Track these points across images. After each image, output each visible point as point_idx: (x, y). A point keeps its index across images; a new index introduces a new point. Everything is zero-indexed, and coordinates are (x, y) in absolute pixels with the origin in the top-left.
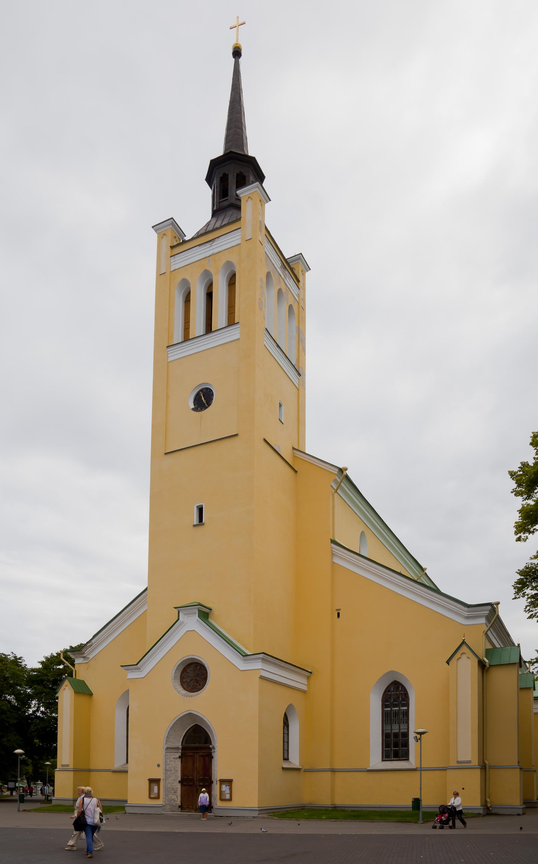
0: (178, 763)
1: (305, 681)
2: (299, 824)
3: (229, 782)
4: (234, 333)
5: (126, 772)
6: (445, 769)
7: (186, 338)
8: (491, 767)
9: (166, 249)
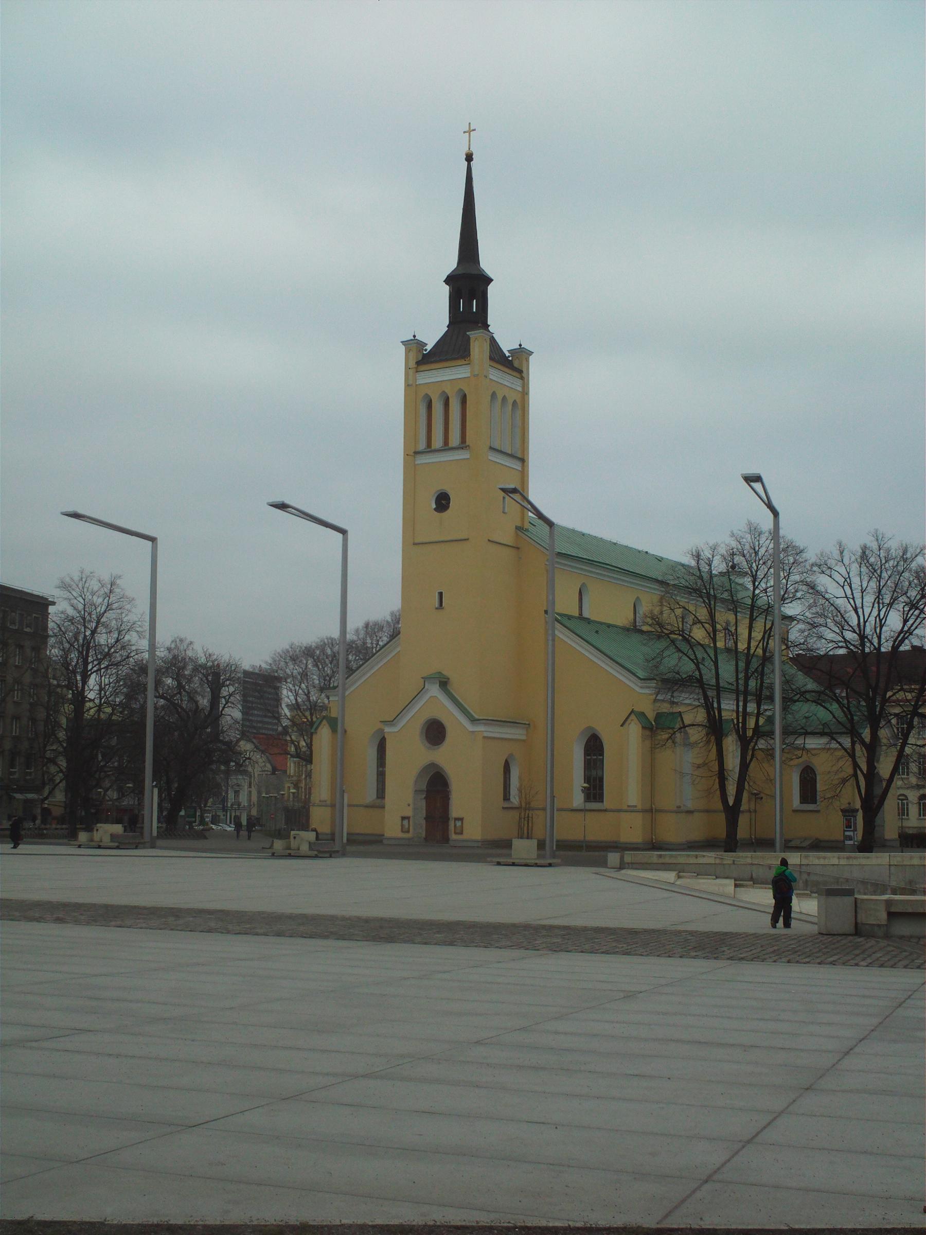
0: (424, 803)
3: (461, 819)
5: (383, 807)
6: (619, 811)
8: (656, 811)
9: (412, 364)
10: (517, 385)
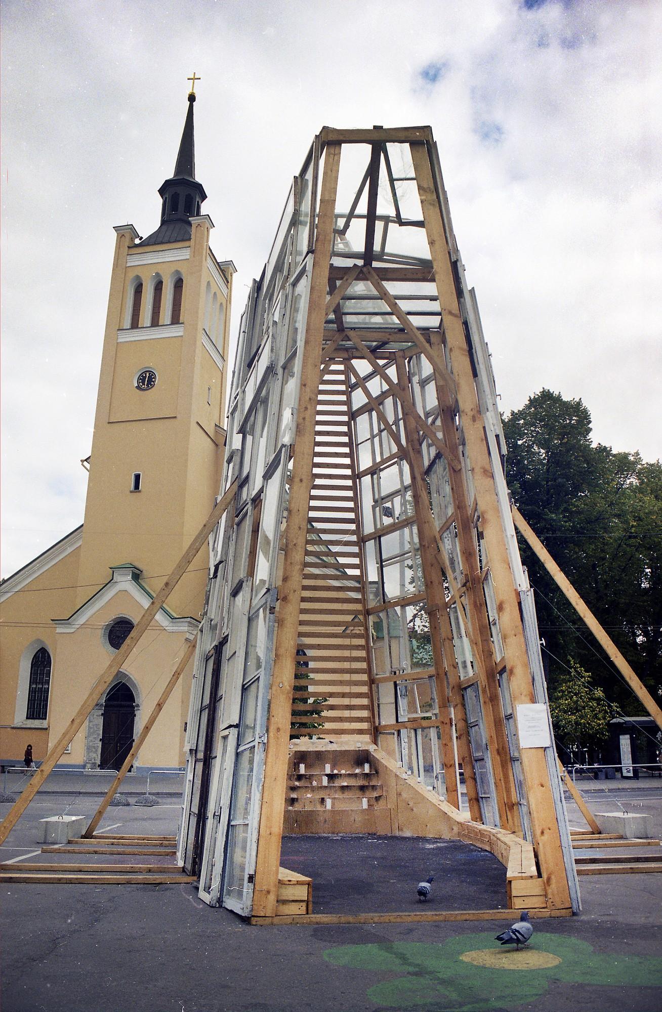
0: (101, 721)
2: (301, 481)
4: (176, 331)
10: (225, 291)
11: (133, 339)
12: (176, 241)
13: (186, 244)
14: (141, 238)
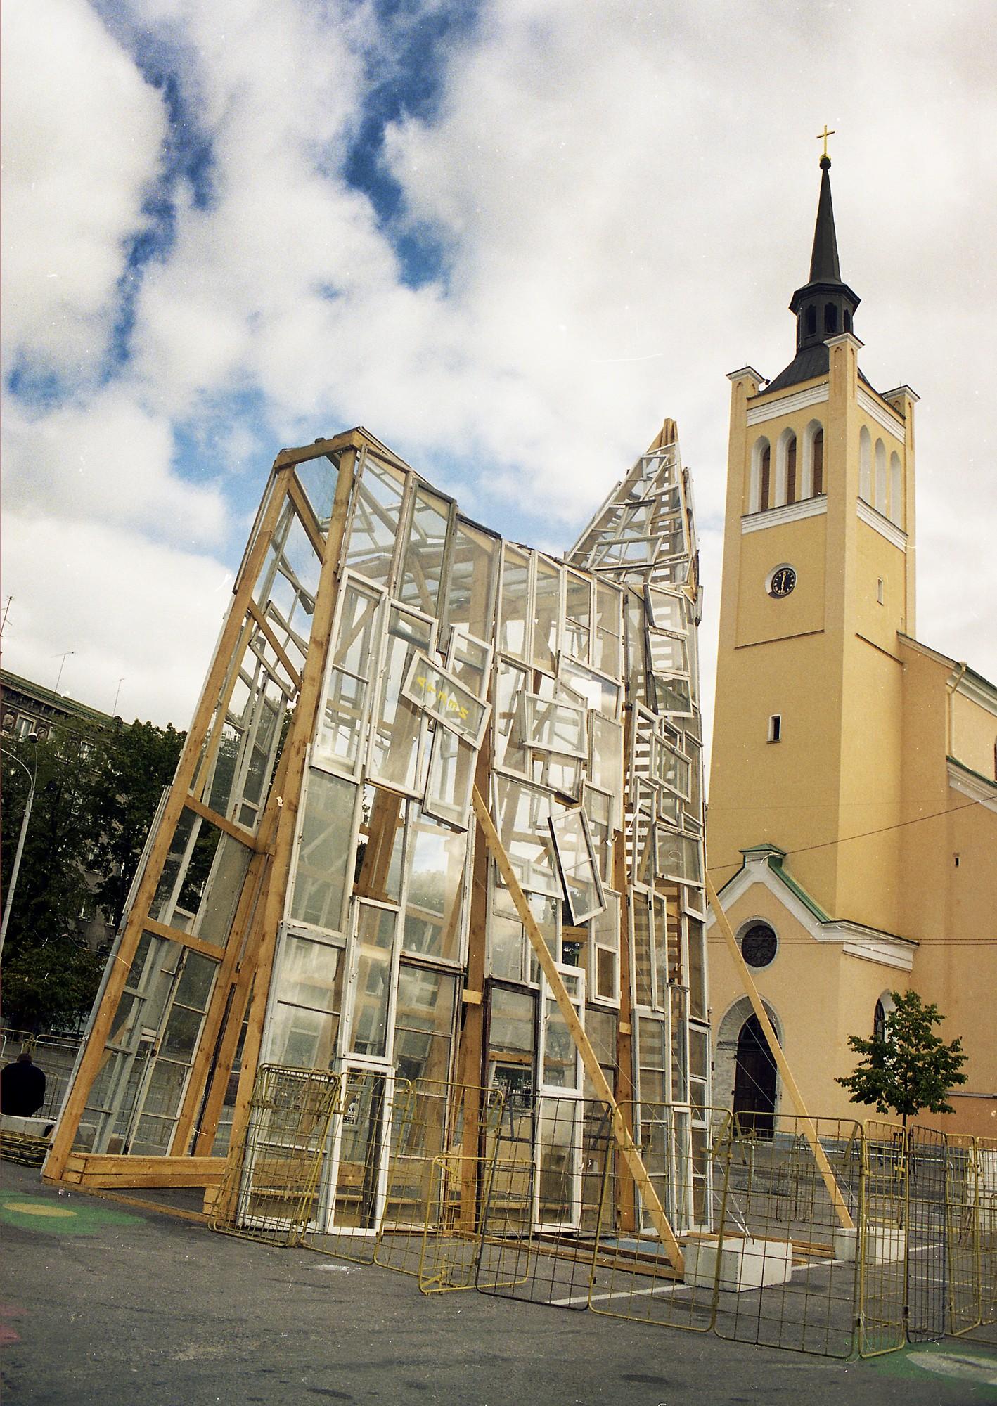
0: (733, 1066)
1: (910, 956)
4: (819, 507)
7: (764, 507)
10: (899, 432)
11: (781, 522)
12: (813, 377)
13: (823, 379)
14: (768, 382)
